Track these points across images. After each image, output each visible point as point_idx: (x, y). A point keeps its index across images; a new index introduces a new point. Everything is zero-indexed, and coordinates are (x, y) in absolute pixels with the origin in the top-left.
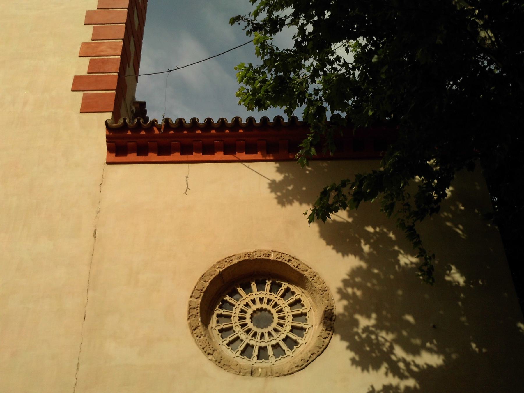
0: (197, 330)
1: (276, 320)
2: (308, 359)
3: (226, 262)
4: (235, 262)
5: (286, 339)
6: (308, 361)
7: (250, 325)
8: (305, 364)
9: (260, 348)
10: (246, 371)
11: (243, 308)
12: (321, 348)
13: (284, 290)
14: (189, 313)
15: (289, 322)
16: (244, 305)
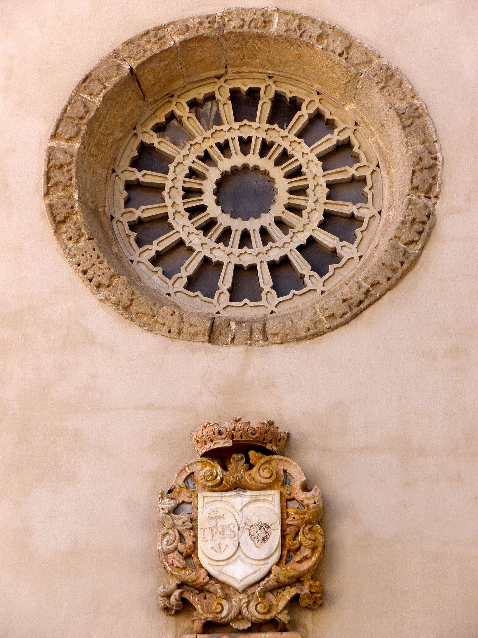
0: (70, 223)
1: (282, 197)
2: (362, 297)
3: (148, 42)
4: (174, 40)
5: (309, 247)
6: (361, 302)
7: (214, 211)
8: (355, 308)
9: (272, 265)
10: (194, 329)
11: (193, 166)
12: (394, 270)
13: (306, 118)
14: (48, 179)
15: (316, 203)
16: (199, 158)
